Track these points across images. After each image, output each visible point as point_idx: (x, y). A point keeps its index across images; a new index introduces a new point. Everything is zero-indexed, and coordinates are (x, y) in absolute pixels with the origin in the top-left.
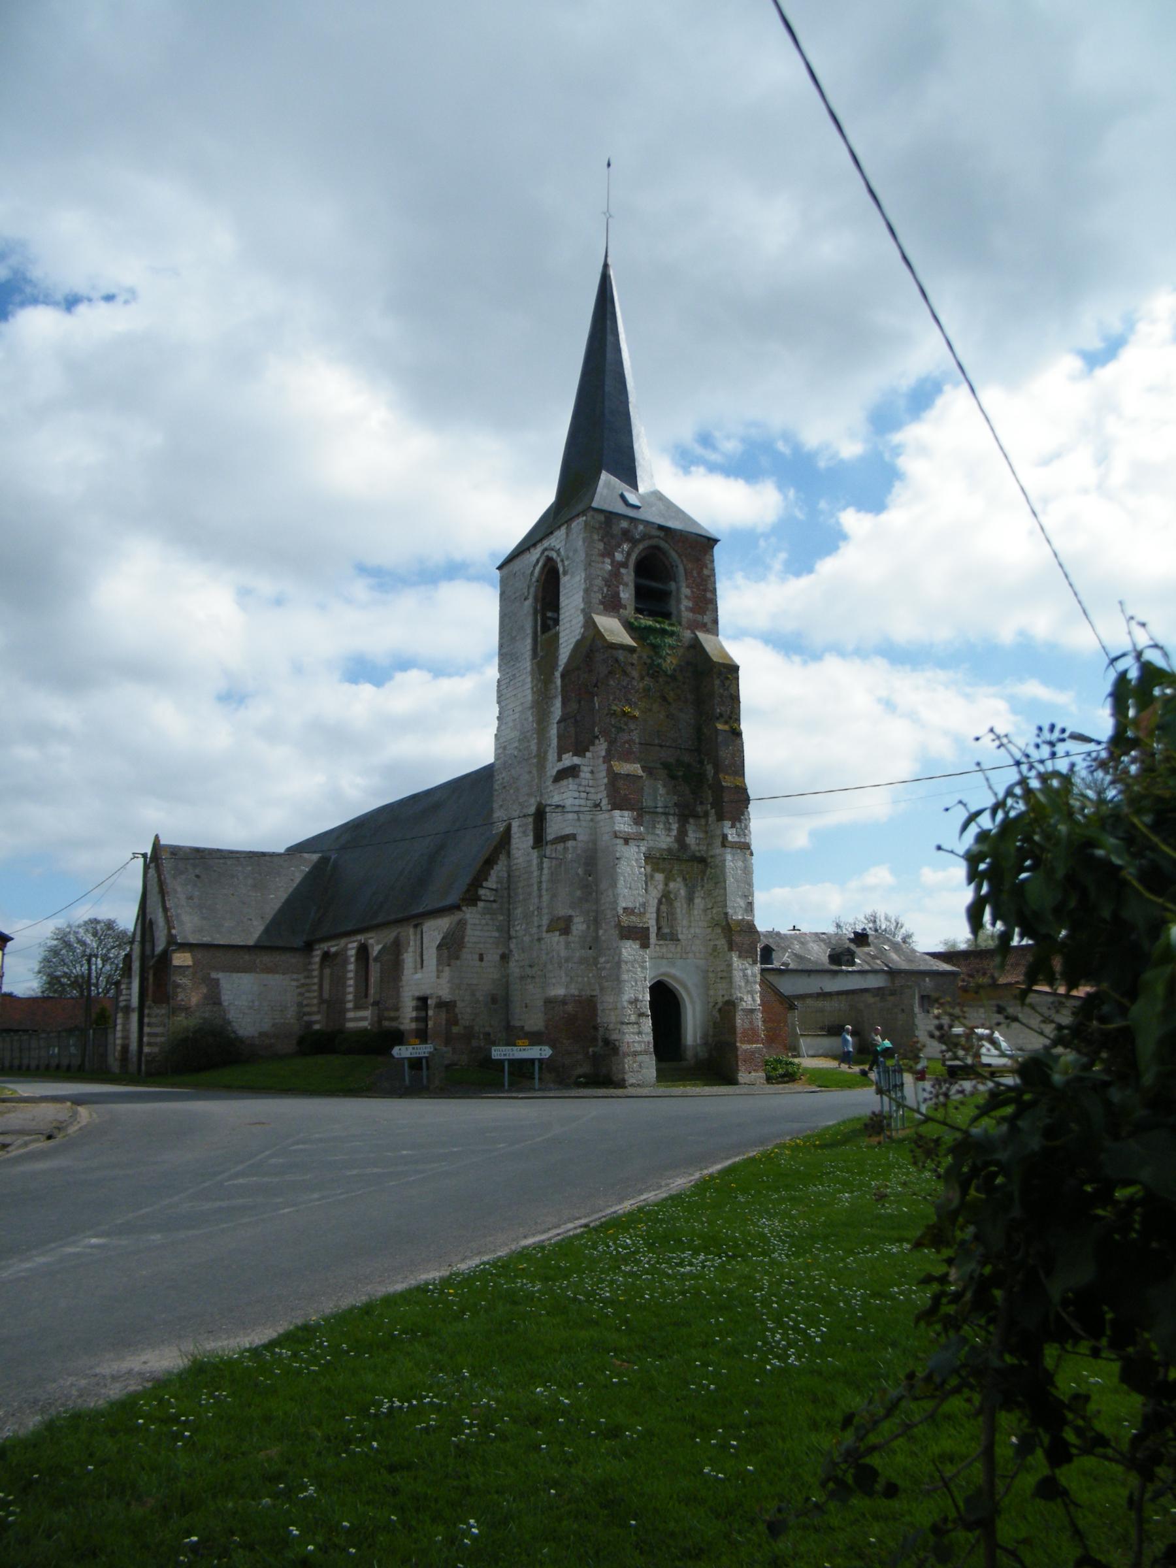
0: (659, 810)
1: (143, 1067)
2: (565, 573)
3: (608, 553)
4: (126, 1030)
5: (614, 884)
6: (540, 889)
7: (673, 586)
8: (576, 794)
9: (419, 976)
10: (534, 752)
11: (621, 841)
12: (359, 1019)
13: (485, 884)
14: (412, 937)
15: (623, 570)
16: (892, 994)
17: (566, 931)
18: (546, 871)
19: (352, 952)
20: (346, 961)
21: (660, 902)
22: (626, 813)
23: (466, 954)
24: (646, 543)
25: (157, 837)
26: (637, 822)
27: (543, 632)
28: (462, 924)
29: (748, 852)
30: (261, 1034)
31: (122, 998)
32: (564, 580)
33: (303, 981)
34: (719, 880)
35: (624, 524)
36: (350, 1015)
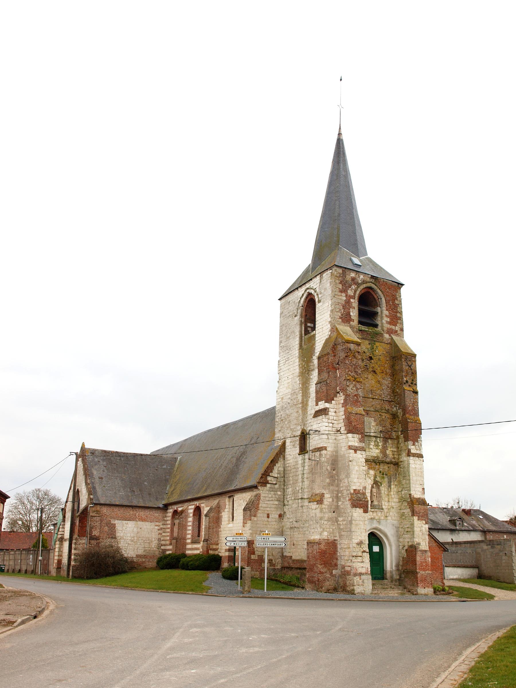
0: (372, 434)
1: (71, 574)
2: (319, 301)
3: (344, 291)
4: (60, 551)
5: (348, 476)
6: (303, 478)
7: (379, 309)
8: (327, 424)
9: (231, 525)
10: (300, 401)
11: (353, 451)
12: (195, 549)
13: (271, 474)
14: (227, 503)
15: (352, 300)
16: (498, 545)
17: (320, 501)
18: (306, 468)
19: (191, 511)
20: (187, 516)
21: (372, 487)
22: (355, 435)
23: (260, 514)
24: (365, 286)
25: (83, 444)
26: (361, 440)
27: (305, 334)
28: (258, 497)
29: (422, 459)
30: (137, 556)
31: (59, 533)
32: (318, 305)
33: (162, 526)
34: (406, 476)
35: (353, 275)
36: (189, 546)
